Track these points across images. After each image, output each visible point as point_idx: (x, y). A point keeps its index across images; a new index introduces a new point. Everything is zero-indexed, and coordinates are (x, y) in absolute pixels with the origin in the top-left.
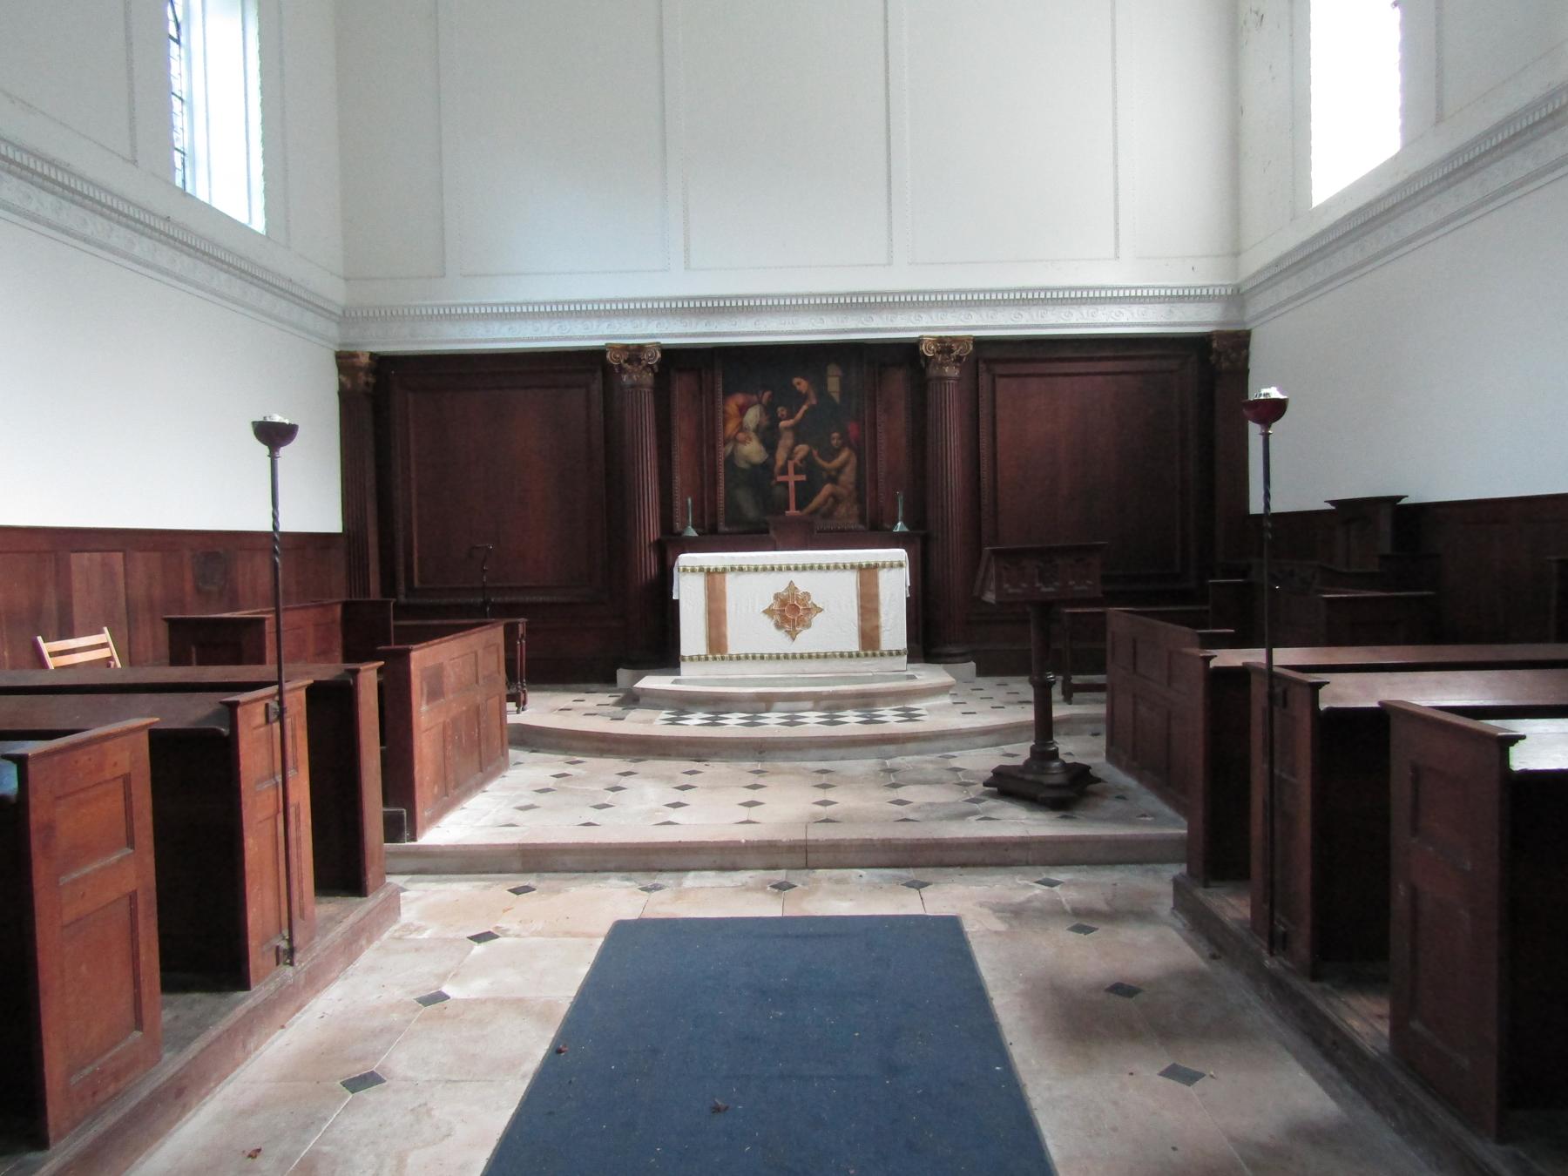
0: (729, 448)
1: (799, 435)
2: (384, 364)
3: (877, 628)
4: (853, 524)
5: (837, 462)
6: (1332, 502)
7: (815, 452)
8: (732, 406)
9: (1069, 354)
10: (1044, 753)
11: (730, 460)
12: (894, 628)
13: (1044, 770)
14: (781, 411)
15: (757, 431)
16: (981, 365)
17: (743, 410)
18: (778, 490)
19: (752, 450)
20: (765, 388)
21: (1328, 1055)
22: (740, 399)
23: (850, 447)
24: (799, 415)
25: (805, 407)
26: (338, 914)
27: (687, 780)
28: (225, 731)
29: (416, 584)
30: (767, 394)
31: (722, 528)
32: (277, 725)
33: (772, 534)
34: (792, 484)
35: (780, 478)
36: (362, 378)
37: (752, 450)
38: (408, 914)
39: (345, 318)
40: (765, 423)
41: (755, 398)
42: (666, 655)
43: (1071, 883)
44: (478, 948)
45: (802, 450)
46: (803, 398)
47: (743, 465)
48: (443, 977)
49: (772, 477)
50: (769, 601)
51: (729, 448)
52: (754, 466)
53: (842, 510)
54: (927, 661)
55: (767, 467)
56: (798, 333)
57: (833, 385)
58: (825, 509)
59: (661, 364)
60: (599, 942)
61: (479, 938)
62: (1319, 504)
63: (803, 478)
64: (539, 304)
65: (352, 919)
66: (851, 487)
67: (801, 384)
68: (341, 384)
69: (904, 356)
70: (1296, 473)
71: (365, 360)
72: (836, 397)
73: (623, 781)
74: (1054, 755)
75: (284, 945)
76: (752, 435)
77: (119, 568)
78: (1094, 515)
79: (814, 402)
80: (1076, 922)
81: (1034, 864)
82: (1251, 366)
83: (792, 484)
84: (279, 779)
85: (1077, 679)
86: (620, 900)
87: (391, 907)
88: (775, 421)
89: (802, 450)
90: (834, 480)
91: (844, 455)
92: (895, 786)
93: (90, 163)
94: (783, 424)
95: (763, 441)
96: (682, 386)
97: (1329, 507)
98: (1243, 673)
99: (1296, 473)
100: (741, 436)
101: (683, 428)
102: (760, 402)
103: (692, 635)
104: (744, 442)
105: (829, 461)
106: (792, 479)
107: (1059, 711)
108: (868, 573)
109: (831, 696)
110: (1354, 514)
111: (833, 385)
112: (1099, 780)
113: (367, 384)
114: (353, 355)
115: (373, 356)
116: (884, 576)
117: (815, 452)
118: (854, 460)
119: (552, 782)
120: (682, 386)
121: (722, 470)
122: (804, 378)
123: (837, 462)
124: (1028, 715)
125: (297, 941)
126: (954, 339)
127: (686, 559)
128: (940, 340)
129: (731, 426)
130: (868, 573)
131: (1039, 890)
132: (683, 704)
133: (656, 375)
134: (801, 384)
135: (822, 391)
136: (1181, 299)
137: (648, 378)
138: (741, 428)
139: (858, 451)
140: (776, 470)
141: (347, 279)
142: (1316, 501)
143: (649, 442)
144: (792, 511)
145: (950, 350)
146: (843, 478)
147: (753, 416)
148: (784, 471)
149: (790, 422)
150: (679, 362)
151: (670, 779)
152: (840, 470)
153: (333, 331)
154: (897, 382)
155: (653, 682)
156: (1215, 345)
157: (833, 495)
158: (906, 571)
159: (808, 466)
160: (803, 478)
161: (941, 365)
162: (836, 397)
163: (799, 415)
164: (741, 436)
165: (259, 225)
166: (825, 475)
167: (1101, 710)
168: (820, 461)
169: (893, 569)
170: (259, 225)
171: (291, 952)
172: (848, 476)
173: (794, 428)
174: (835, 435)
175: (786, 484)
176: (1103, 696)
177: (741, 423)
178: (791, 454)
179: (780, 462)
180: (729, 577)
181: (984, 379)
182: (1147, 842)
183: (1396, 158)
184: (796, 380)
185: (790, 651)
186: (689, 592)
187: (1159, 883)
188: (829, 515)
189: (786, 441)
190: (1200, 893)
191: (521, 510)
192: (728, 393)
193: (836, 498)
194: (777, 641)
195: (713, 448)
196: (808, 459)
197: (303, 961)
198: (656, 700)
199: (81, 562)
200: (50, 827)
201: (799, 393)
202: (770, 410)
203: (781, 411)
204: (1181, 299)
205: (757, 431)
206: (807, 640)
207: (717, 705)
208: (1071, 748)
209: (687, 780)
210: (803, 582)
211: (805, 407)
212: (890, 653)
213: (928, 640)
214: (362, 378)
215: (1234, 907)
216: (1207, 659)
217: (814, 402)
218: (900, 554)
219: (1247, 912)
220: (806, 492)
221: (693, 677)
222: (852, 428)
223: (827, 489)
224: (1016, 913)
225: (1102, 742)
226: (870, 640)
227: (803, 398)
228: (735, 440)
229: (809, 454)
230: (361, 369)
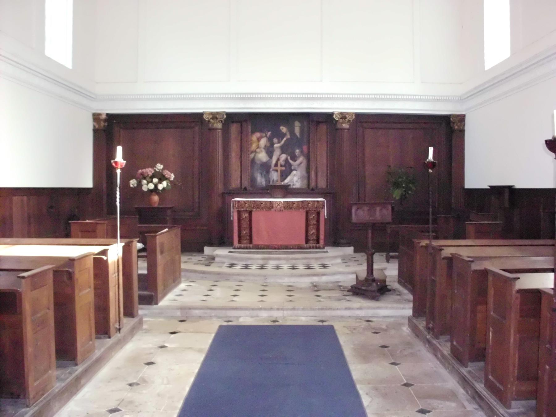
0: (252, 156)
1: (283, 150)
2: (111, 118)
6: (490, 186)
7: (289, 158)
8: (254, 137)
11: (253, 161)
14: (275, 140)
17: (259, 140)
19: (262, 156)
21: (228, 155)
22: (258, 134)
23: (304, 156)
24: (283, 142)
25: (285, 139)
26: (128, 323)
27: (238, 288)
36: (102, 124)
37: (262, 156)
41: (264, 135)
44: (173, 336)
45: (284, 157)
46: (284, 135)
48: (164, 342)
54: (333, 246)
56: (281, 109)
57: (297, 130)
59: (225, 120)
60: (213, 335)
62: (485, 186)
63: (284, 168)
64: (173, 94)
67: (284, 129)
68: (94, 126)
70: (481, 171)
71: (104, 117)
73: (213, 288)
75: (118, 327)
76: (263, 150)
77: (25, 202)
78: (395, 188)
79: (289, 137)
82: (467, 128)
84: (117, 274)
88: (272, 144)
89: (284, 157)
92: (317, 291)
95: (267, 153)
96: (234, 128)
97: (489, 188)
99: (481, 171)
100: (258, 150)
101: (234, 146)
102: (266, 136)
104: (259, 153)
110: (497, 191)
111: (297, 130)
113: (104, 126)
114: (100, 114)
115: (107, 115)
118: (305, 162)
119: (186, 288)
125: (121, 327)
128: (341, 113)
129: (254, 146)
133: (223, 124)
134: (284, 129)
135: (292, 132)
136: (438, 100)
137: (219, 126)
142: (484, 185)
143: (220, 151)
145: (345, 118)
147: (263, 142)
149: (279, 145)
150: (232, 119)
151: (230, 287)
156: (451, 119)
160: (284, 168)
161: (342, 123)
163: (283, 142)
164: (258, 150)
165: (69, 65)
168: (291, 162)
170: (69, 65)
171: (119, 329)
183: (508, 59)
184: (281, 127)
189: (277, 153)
190: (415, 321)
191: (171, 182)
192: (253, 132)
199: (16, 199)
200: (77, 279)
202: (270, 140)
203: (275, 140)
204: (438, 100)
211: (285, 139)
214: (102, 124)
217: (289, 137)
222: (305, 148)
227: (284, 135)
228: (255, 152)
230: (101, 120)
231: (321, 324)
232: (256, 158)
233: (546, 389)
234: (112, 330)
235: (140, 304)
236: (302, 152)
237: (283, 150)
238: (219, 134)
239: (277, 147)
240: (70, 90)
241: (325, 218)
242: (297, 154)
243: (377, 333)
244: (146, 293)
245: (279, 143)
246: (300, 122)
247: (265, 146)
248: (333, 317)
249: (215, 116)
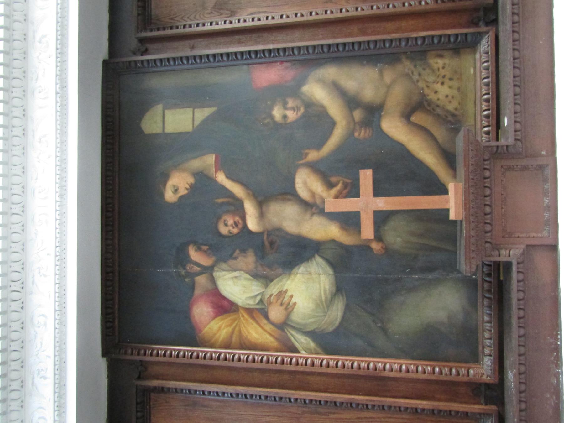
0: (301, 341)
4: (476, 65)
5: (335, 109)
8: (216, 328)
11: (327, 341)
14: (227, 226)
15: (267, 280)
17: (224, 307)
18: (397, 237)
19: (307, 291)
20: (182, 258)
22: (201, 311)
23: (302, 81)
24: (237, 190)
25: (221, 178)
30: (194, 254)
31: (485, 370)
33: (511, 254)
34: (383, 204)
35: (368, 231)
37: (307, 291)
40: (249, 260)
41: (202, 280)
45: (306, 183)
46: (203, 181)
47: (337, 312)
49: (365, 248)
51: (301, 341)
52: (339, 288)
53: (442, 93)
55: (342, 260)
58: (440, 133)
63: (366, 177)
66: (389, 76)
72: (202, 114)
76: (274, 289)
79: (210, 159)
83: (383, 204)
88: (246, 240)
89: (306, 183)
90: (373, 112)
93: (259, 322)
94: (252, 224)
100: (276, 314)
102: (208, 270)
104: (289, 308)
105: (333, 124)
106: (368, 203)
112: (212, 303)
117: (313, 155)
118: (330, 72)
121: (346, 360)
122: (166, 177)
123: (335, 109)
129: (256, 332)
138: (259, 312)
140: (346, 239)
146: (369, 94)
147: (237, 286)
148: (350, 221)
149: (250, 208)
152: (351, 102)
157: (407, 115)
159: (340, 172)
162: (202, 114)
163: (237, 190)
166: (362, 134)
172: (363, 81)
173: (261, 203)
174: (277, 113)
177: (250, 311)
178: (311, 207)
179: (333, 231)
184: (170, 196)
187: (153, 21)
188: (453, 122)
189: (288, 218)
192: (191, 337)
193: (417, 107)
195: (299, 379)
201: (193, 188)
202: (224, 249)
203: (227, 226)
205: (267, 280)
211: (221, 178)
220: (399, 173)
223: (394, 128)
227: (203, 181)
228: (283, 326)
229: (315, 168)
232: (312, 324)
233: (329, 395)
236: (282, 92)
239: (262, 215)
240: (519, 83)
242: (292, 115)
245: (237, 207)
246: (143, 107)
247: (256, 276)
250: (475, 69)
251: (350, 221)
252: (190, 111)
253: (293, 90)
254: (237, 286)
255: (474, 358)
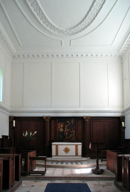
3: (78, 152)
4: (75, 139)
5: (72, 132)
9: (102, 118)
10: (98, 168)
12: (80, 153)
13: (98, 170)
14: (65, 125)
16: (91, 120)
17: (60, 125)
19: (62, 130)
22: (60, 123)
26: (16, 183)
27: (54, 170)
28: (8, 160)
29: (18, 145)
31: (57, 140)
32: (13, 160)
33: (64, 140)
37: (62, 130)
38: (23, 185)
39: (11, 112)
42: (50, 155)
43: (102, 182)
44: (32, 187)
45: (68, 130)
50: (64, 149)
55: (64, 132)
57: (72, 122)
59: (50, 119)
60: (46, 187)
61: (32, 186)
65: (18, 183)
67: (68, 122)
69: (82, 118)
74: (99, 168)
80: (102, 186)
81: (98, 180)
85: (103, 159)
86: (49, 182)
87: (21, 183)
88: (65, 126)
89: (68, 130)
90: (72, 134)
91: (74, 131)
95: (63, 129)
96: (53, 121)
98: (121, 157)
100: (60, 128)
103: (54, 153)
106: (67, 134)
107: (99, 163)
108: (77, 146)
109: (72, 161)
111: (72, 122)
116: (79, 146)
118: (75, 131)
120: (53, 121)
124: (96, 164)
126: (88, 117)
127: (53, 143)
130: (77, 146)
131: (98, 183)
132: (53, 161)
134: (68, 122)
135: (71, 123)
139: (76, 131)
141: (11, 107)
144: (67, 138)
147: (62, 125)
150: (52, 118)
152: (73, 133)
153: (9, 114)
154: (80, 122)
155: (48, 159)
158: (81, 145)
159: (69, 132)
164: (60, 128)
167: (106, 163)
169: (80, 145)
171: (13, 186)
172: (74, 133)
175: (66, 134)
176: (106, 161)
180: (59, 146)
181: (92, 122)
182: (111, 177)
185: (66, 155)
186: (54, 148)
187: (113, 182)
188: (71, 138)
189: (66, 129)
190: (117, 182)
192: (59, 123)
193: (72, 136)
194: (65, 154)
196: (69, 131)
197: (14, 187)
198: (50, 161)
202: (64, 125)
206: (69, 154)
207: (57, 162)
208: (101, 168)
209: (54, 170)
210: (68, 147)
212: (79, 156)
213: (84, 155)
215: (121, 184)
216: (118, 155)
218: (80, 143)
219: (122, 184)
221: (54, 158)
222: (75, 127)
224: (95, 185)
225: (106, 167)
226: (77, 154)
229: (69, 130)
231: (83, 183)
234: (10, 186)
235: (21, 176)
237: (68, 128)
238: (48, 123)
241: (124, 121)
243: (104, 187)
244: (24, 172)
248: (110, 180)
249: (47, 117)
250: (76, 127)
251: (66, 133)
252: (52, 146)
253: (74, 129)
254: (62, 125)
255: (59, 139)
